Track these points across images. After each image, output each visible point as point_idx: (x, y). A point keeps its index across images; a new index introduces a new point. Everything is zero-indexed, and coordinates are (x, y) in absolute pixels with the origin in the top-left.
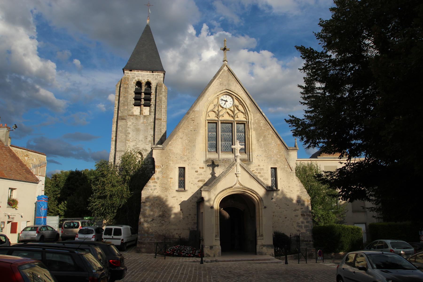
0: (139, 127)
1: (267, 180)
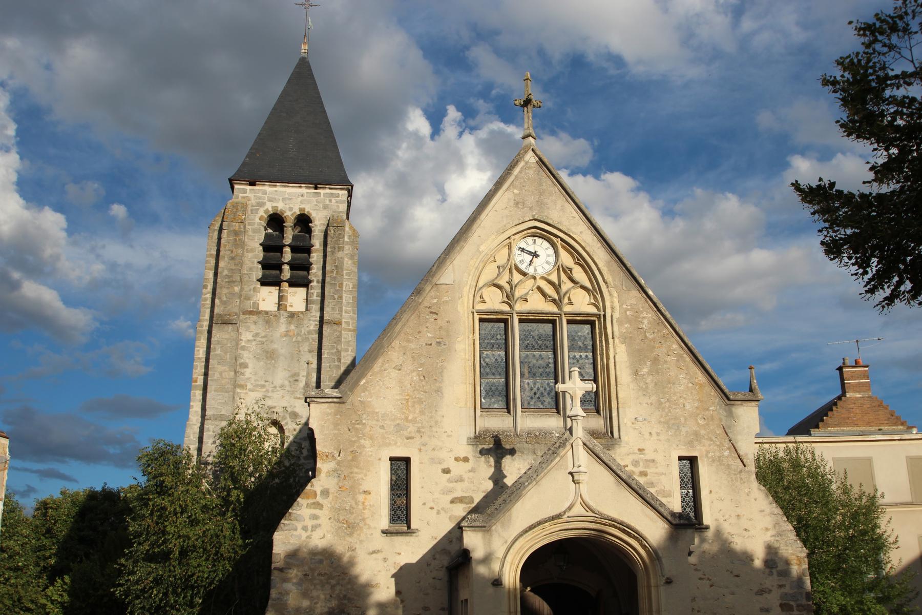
0: (275, 346)
1: (669, 495)
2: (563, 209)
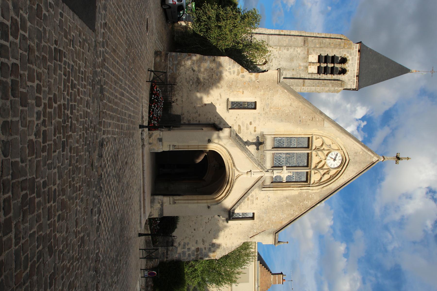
0: (295, 61)
1: (240, 209)
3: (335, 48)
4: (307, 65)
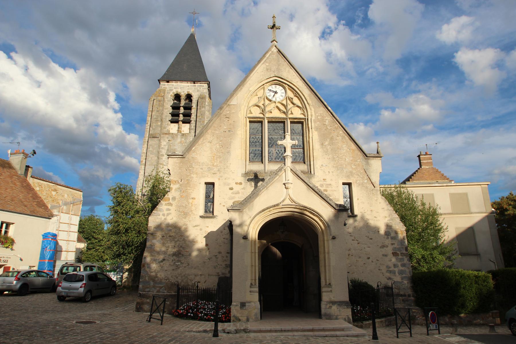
0: (176, 147)
2: (289, 72)
3: (163, 106)
4: (180, 134)
